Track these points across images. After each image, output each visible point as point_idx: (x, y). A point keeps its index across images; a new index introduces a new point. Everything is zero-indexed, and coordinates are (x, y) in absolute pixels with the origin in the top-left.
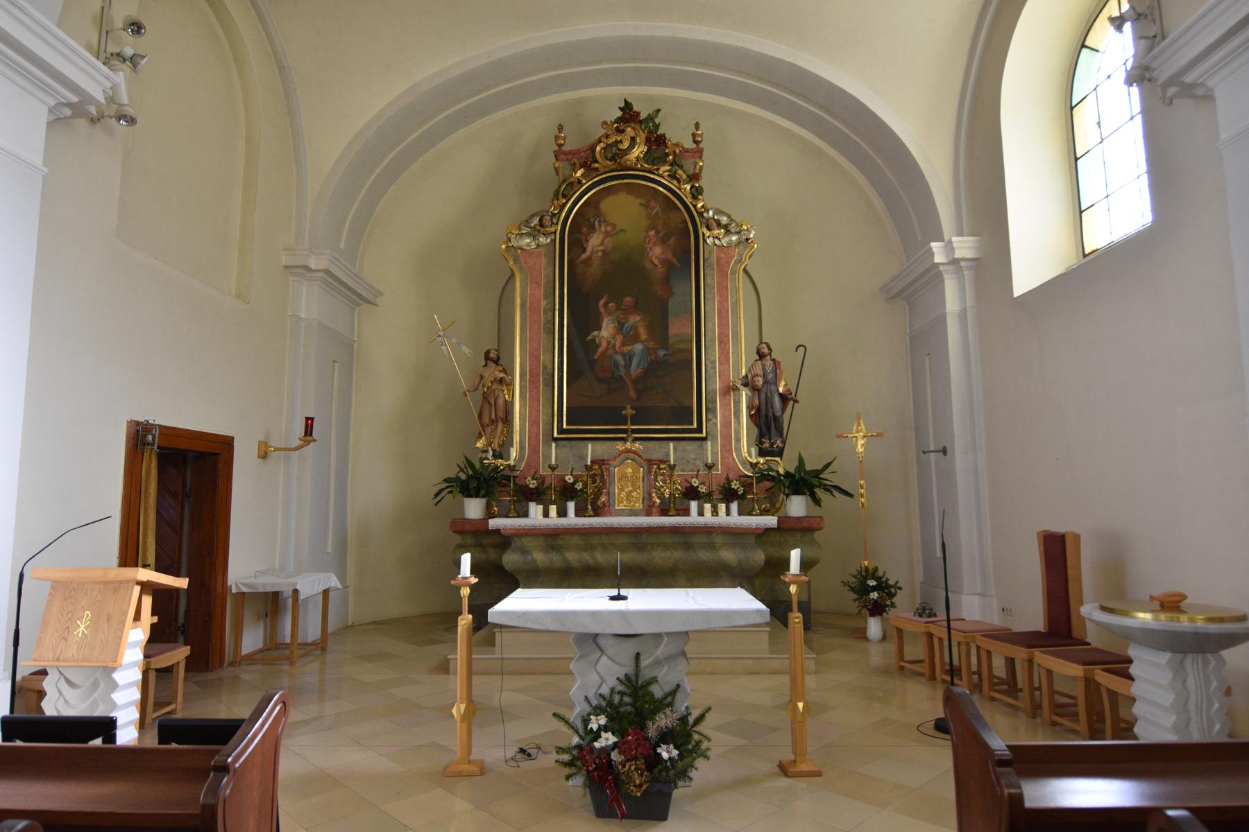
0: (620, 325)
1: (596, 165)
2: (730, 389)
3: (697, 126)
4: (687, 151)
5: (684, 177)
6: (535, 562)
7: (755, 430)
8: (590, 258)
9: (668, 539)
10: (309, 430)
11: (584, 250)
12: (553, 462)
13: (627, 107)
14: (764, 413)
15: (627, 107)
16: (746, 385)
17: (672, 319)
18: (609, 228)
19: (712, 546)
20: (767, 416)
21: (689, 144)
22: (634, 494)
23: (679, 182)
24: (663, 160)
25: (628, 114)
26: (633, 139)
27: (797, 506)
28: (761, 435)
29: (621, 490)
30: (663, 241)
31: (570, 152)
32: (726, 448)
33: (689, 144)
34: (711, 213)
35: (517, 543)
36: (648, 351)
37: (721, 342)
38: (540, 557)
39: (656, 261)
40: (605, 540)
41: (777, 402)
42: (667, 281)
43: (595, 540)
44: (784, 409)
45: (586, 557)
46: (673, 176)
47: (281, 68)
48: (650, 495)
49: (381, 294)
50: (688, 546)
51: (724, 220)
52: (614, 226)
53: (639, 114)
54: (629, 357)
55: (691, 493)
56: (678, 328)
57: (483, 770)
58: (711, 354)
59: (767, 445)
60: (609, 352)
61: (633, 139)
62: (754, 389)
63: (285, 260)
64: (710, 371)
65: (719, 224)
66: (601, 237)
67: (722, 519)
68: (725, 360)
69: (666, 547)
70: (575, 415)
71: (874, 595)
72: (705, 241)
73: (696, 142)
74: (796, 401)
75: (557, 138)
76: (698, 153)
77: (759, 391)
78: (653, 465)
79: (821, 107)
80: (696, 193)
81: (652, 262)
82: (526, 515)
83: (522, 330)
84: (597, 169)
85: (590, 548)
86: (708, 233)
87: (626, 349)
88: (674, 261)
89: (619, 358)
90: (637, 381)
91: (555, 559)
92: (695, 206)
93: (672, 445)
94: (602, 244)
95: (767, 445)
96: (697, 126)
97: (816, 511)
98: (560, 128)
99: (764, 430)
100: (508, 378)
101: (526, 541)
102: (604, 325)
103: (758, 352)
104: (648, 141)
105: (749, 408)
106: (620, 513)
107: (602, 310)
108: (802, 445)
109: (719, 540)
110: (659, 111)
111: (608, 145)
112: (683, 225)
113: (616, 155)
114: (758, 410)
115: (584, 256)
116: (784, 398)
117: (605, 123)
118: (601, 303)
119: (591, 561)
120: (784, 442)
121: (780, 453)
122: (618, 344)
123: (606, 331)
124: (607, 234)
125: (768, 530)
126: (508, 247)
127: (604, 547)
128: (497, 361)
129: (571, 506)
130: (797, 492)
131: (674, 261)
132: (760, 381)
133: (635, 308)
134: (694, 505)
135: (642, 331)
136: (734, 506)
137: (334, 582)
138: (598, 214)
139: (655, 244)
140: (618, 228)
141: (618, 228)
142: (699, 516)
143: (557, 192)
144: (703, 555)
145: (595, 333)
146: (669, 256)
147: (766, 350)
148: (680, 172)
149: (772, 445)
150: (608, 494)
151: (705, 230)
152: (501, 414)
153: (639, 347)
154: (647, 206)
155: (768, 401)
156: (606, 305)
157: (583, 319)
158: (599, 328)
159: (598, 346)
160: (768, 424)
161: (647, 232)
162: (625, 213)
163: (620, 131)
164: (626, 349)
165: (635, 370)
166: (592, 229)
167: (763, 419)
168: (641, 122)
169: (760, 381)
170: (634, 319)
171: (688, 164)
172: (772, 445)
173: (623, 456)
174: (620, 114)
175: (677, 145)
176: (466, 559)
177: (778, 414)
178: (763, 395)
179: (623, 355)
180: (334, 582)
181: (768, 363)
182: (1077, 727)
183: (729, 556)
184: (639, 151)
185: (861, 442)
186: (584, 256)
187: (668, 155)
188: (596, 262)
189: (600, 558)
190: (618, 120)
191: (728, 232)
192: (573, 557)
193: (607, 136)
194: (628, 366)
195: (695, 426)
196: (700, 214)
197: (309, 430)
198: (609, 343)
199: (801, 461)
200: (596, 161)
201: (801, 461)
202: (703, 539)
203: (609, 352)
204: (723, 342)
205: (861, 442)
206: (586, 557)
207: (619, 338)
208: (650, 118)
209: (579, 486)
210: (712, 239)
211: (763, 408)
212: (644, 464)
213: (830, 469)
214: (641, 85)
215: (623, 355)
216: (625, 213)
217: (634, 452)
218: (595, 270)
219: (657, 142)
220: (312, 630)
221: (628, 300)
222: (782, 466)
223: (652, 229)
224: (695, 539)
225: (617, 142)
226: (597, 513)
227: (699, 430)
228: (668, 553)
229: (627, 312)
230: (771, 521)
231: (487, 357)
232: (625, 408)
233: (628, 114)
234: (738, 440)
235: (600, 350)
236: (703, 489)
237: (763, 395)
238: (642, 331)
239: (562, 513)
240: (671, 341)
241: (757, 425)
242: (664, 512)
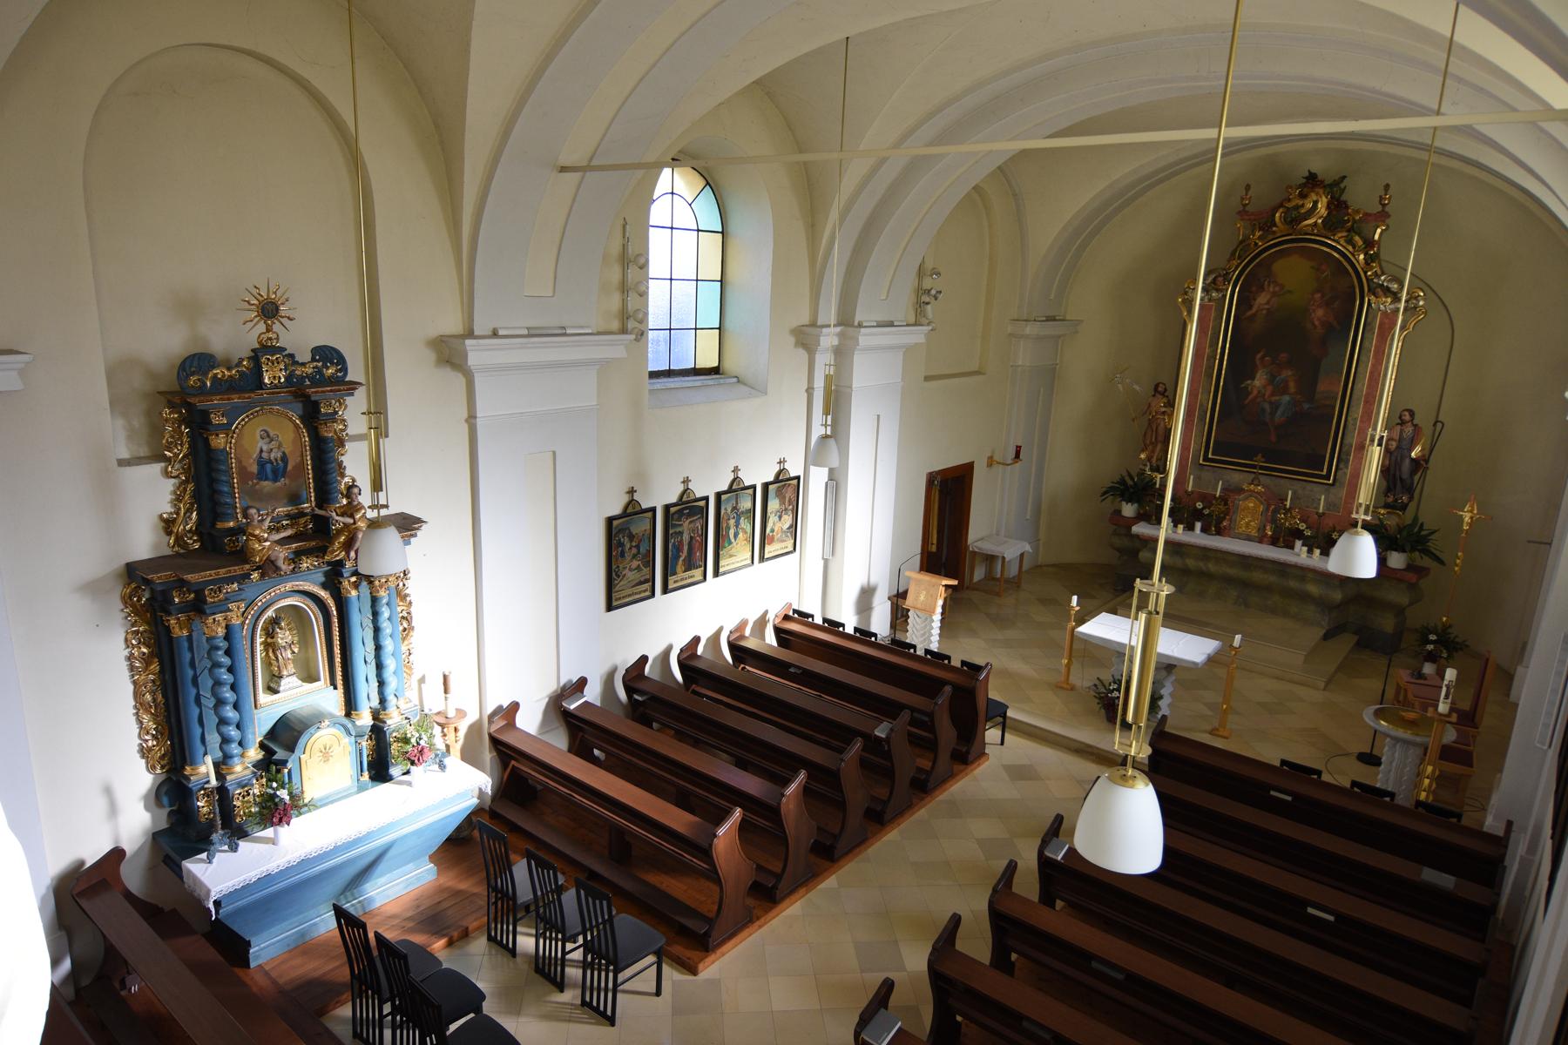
0: (1272, 379)
3: (1387, 187)
4: (1366, 214)
5: (1360, 243)
8: (1254, 315)
10: (1017, 455)
11: (1251, 307)
25: (1312, 181)
26: (1315, 203)
37: (1366, 402)
45: (1201, 564)
46: (1350, 241)
47: (1015, 195)
52: (1282, 287)
55: (1298, 534)
57: (1073, 688)
63: (1009, 329)
64: (1350, 426)
71: (1430, 647)
78: (1274, 502)
89: (1267, 406)
98: (1248, 187)
109: (1310, 575)
113: (1294, 219)
116: (1417, 464)
120: (1411, 499)
123: (1259, 381)
124: (1274, 294)
128: (1163, 394)
129: (1198, 525)
135: (1292, 385)
137: (1028, 548)
143: (1233, 254)
144: (1293, 584)
147: (1407, 417)
148: (1357, 238)
152: (1161, 438)
153: (1286, 398)
157: (1241, 364)
159: (1249, 393)
162: (1294, 274)
163: (1303, 196)
165: (1279, 417)
166: (1261, 288)
170: (1287, 373)
175: (1358, 212)
176: (1075, 598)
180: (1028, 548)
181: (1409, 429)
182: (1117, 742)
183: (1313, 589)
185: (1467, 519)
189: (1212, 567)
192: (1191, 563)
197: (1017, 455)
205: (1467, 519)
207: (1270, 388)
219: (1338, 205)
220: (1013, 571)
221: (1284, 356)
226: (1219, 532)
231: (1156, 389)
238: (1292, 385)
239: (1190, 528)
242: (1274, 542)
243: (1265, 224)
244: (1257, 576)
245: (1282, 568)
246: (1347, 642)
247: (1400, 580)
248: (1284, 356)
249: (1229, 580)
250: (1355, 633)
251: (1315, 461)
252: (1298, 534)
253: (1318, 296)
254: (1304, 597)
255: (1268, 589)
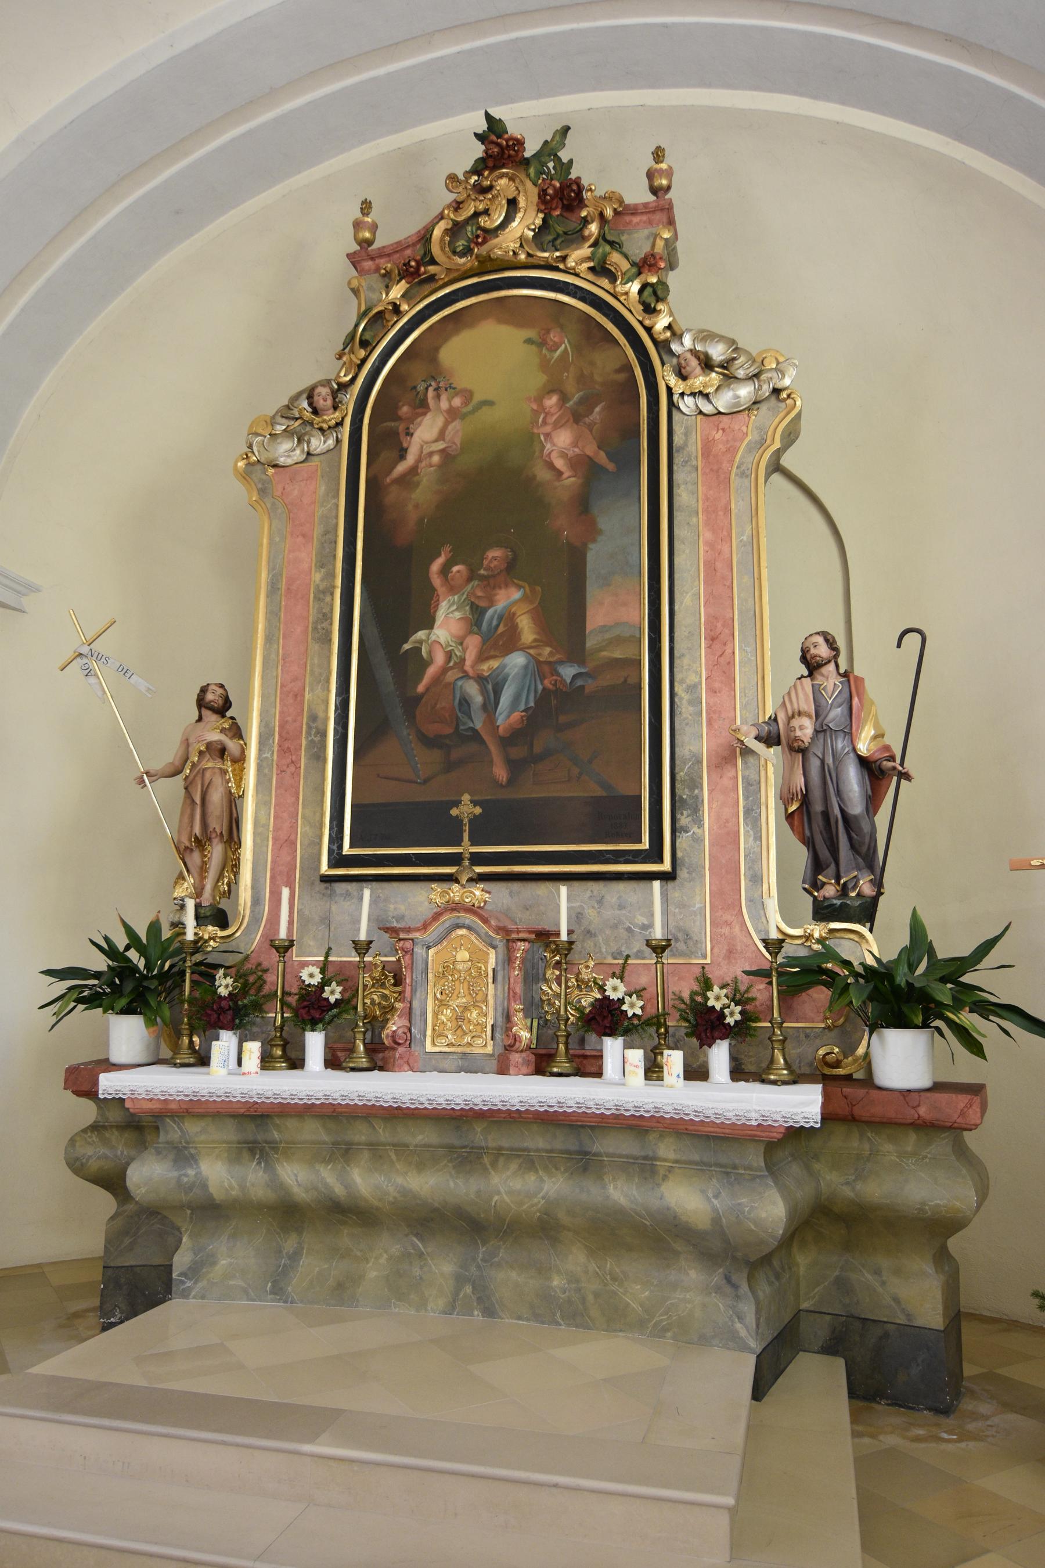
0: (476, 613)
1: (432, 269)
2: (734, 752)
3: (658, 155)
4: (633, 210)
5: (625, 265)
6: (204, 1186)
7: (801, 855)
8: (414, 470)
9: (537, 1141)
12: (283, 934)
13: (493, 131)
14: (818, 807)
15: (493, 131)
16: (770, 739)
17: (593, 592)
18: (457, 402)
19: (646, 1169)
20: (826, 815)
21: (638, 194)
22: (474, 1014)
23: (613, 279)
24: (577, 237)
25: (499, 149)
26: (512, 203)
27: (902, 1059)
28: (817, 866)
29: (441, 1004)
30: (577, 417)
31: (382, 253)
32: (726, 900)
33: (638, 194)
34: (688, 340)
35: (172, 1132)
36: (539, 668)
37: (712, 639)
38: (217, 1174)
39: (559, 463)
40: (383, 1133)
41: (853, 779)
42: (582, 506)
43: (360, 1133)
44: (873, 802)
46: (601, 270)
48: (508, 1017)
49: (32, 589)
50: (584, 1164)
51: (717, 352)
52: (468, 395)
53: (520, 143)
54: (493, 687)
55: (607, 1018)
56: (613, 610)
58: (692, 666)
59: (830, 891)
60: (450, 676)
61: (512, 203)
62: (798, 750)
64: (685, 709)
65: (707, 364)
66: (440, 421)
67: (675, 1094)
68: (728, 689)
69: (529, 1161)
70: (373, 823)
72: (671, 405)
73: (654, 191)
74: (907, 776)
75: (357, 225)
76: (661, 205)
77: (803, 751)
79: (951, 41)
80: (653, 298)
81: (551, 466)
82: (203, 1060)
83: (269, 639)
84: (432, 278)
85: (343, 1152)
86: (678, 386)
87: (485, 668)
88: (602, 458)
89: (472, 689)
90: (510, 740)
91: (251, 1180)
92: (649, 330)
93: (367, 893)
94: (441, 436)
95: (830, 891)
96: (658, 155)
97: (965, 1068)
98: (366, 207)
99: (824, 853)
100: (232, 745)
101: (192, 1128)
102: (441, 614)
103: (804, 659)
104: (544, 202)
105: (785, 798)
106: (437, 1064)
107: (436, 581)
108: (931, 886)
109: (667, 1150)
110: (566, 129)
111: (456, 224)
112: (622, 377)
114: (805, 800)
115: (401, 468)
117: (452, 178)
118: (436, 566)
119: (339, 1190)
120: (878, 884)
121: (867, 913)
122: (470, 656)
123: (445, 630)
124: (453, 414)
125: (796, 1134)
126: (249, 464)
127: (377, 1152)
129: (315, 1043)
130: (902, 1022)
131: (602, 458)
132: (805, 729)
133: (511, 571)
134: (612, 1047)
136: (719, 1055)
138: (436, 373)
139: (557, 426)
140: (478, 398)
141: (478, 398)
142: (622, 1080)
144: (620, 1193)
145: (421, 634)
146: (591, 449)
147: (823, 651)
149: (844, 891)
150: (410, 1013)
151: (673, 380)
152: (217, 824)
153: (517, 661)
154: (542, 343)
155: (831, 777)
156: (445, 571)
158: (429, 623)
159: (425, 664)
160: (835, 842)
161: (539, 399)
164: (485, 668)
165: (508, 714)
166: (422, 406)
167: (818, 822)
168: (526, 162)
169: (805, 729)
170: (509, 597)
171: (638, 242)
172: (844, 891)
173: (447, 919)
174: (478, 150)
175: (608, 198)
177: (856, 807)
178: (815, 764)
179: (481, 680)
181: (830, 680)
183: (688, 1198)
184: (525, 224)
186: (401, 468)
187: (586, 222)
188: (428, 477)
189: (364, 1181)
190: (477, 170)
191: (730, 378)
192: (297, 1177)
193: (458, 206)
194: (490, 706)
195: (645, 844)
196: (663, 347)
198: (449, 655)
199: (917, 929)
200: (433, 262)
201: (917, 929)
202: (624, 1145)
203: (450, 676)
204: (718, 638)
206: (329, 1179)
207: (473, 642)
208: (549, 150)
209: (333, 993)
210: (694, 404)
211: (816, 794)
212: (497, 938)
213: (988, 961)
214: (539, 96)
215: (481, 680)
216: (494, 367)
217: (471, 910)
218: (423, 496)
219: (564, 199)
221: (495, 555)
222: (870, 946)
223: (551, 392)
224: (608, 1145)
225: (476, 214)
226: (380, 1057)
227: (655, 854)
228: (531, 1178)
229: (491, 583)
230: (805, 1104)
231: (201, 703)
232: (457, 803)
233: (499, 149)
234: (756, 879)
235: (431, 671)
236: (633, 1007)
237: (815, 764)
240: (590, 643)
241: (809, 842)
242: (542, 1064)
243: (414, 266)
244: (512, 1187)
245: (577, 1137)
246: (819, 1384)
247: (928, 1128)
248: (495, 555)
249: (427, 1221)
250: (830, 1349)
251: (614, 816)
252: (607, 1018)
253: (552, 401)
254: (661, 1238)
255: (544, 1229)
